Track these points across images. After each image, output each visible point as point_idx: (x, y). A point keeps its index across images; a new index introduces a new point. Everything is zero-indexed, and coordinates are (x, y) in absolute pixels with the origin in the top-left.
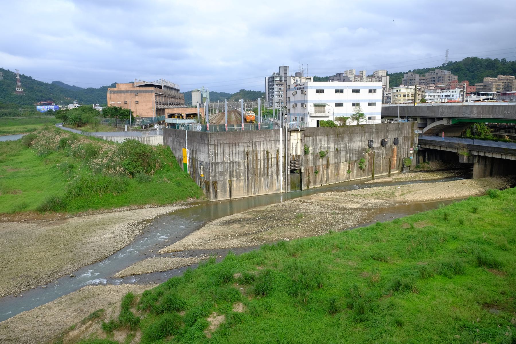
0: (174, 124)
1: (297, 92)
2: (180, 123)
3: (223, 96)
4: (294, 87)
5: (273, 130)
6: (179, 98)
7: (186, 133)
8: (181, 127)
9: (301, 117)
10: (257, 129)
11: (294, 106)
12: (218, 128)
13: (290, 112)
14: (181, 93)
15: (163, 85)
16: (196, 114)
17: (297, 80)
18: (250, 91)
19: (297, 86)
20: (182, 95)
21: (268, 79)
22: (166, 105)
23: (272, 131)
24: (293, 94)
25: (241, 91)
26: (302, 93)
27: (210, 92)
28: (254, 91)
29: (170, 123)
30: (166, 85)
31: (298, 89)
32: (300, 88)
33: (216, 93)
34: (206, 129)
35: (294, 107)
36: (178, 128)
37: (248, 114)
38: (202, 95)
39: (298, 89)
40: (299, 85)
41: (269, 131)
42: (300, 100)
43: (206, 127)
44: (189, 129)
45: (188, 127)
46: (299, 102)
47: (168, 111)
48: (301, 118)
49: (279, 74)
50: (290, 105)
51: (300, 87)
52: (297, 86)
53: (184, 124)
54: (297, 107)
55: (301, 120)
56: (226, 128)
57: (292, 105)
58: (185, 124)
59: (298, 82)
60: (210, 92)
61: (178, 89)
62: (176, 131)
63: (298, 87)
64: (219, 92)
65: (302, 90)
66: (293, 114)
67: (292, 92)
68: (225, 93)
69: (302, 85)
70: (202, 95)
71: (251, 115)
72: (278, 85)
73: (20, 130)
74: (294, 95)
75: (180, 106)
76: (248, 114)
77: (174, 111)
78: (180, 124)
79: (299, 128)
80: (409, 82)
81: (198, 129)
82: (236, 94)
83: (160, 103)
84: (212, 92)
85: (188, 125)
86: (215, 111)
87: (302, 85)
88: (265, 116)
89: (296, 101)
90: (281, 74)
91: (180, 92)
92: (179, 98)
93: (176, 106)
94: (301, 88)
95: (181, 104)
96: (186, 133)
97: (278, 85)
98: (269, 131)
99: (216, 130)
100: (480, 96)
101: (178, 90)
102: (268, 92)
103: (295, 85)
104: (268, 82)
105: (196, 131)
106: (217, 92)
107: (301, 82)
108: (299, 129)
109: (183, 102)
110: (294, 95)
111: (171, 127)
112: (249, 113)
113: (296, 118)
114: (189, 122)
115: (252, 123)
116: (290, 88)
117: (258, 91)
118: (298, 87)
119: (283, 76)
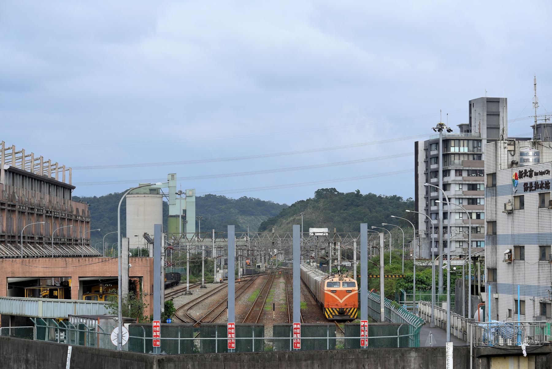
0: (27, 320)
1: (521, 198)
2: (49, 316)
3: (252, 214)
4: (510, 182)
5: (417, 350)
6: (71, 218)
7: (69, 356)
8: (52, 331)
9: (537, 300)
10: (357, 343)
11: (510, 257)
12: (198, 342)
13: (495, 280)
14: (77, 199)
15: (7, 167)
16: (113, 282)
17: (522, 154)
18: (357, 195)
19: (521, 175)
20: (81, 207)
21: (426, 150)
22: (12, 243)
23: (413, 354)
24: (509, 208)
25: (319, 193)
26: (542, 204)
27: (196, 198)
28: (371, 197)
29: (13, 317)
30: (18, 165)
31: (526, 190)
32: (536, 183)
33: (222, 200)
34: (149, 342)
35: (510, 260)
36: (41, 333)
37: (330, 285)
38: (165, 207)
39: (528, 188)
40: (531, 171)
41: (398, 356)
42: (536, 232)
43: (149, 334)
44: (86, 339)
45: (82, 335)
46: (530, 238)
47: (9, 269)
48: (538, 305)
49: (469, 131)
50: (495, 251)
51: (534, 179)
52: (521, 175)
53: (66, 320)
54: (522, 258)
55: (538, 311)
56: (231, 337)
57: (504, 250)
58: (72, 321)
59: (527, 160)
60: (196, 198)
61: (67, 182)
62: (28, 348)
63: (526, 180)
64: (236, 196)
65: (544, 191)
66: (511, 289)
67: (504, 199)
68: (259, 204)
69: (542, 173)
70: (165, 207)
71: (341, 288)
72: (465, 174)
73: (517, 211)
74: (510, 213)
75: (70, 251)
76: (330, 285)
77: (37, 270)
78: (50, 320)
79: (524, 346)
80: (75, 243)
81: (115, 343)
82: (301, 206)
83: (13, 237)
84: (209, 197)
85: (82, 326)
86: (210, 271)
87: (542, 173)
88: (402, 295)
89: (519, 235)
90: (474, 133)
91: (74, 193)
92: (71, 218)
93: (52, 250)
94: (538, 186)
95: (77, 242)
96: (69, 356)
97: (465, 174)
98: (398, 356)
99: (188, 347)
100: (538, 175)
101: (69, 188)
102: (426, 198)
103: (516, 170)
104: (426, 162)
105: (107, 351)
106: (229, 196)
107: (538, 161)
108: (524, 348)
109: (83, 232)
110: (510, 213)
111: (18, 333)
112: (336, 279)
113: (520, 305)
114: (85, 313)
115: (344, 321)
116: (494, 185)
117: (390, 194)
118: (526, 180)
119: (484, 136)
